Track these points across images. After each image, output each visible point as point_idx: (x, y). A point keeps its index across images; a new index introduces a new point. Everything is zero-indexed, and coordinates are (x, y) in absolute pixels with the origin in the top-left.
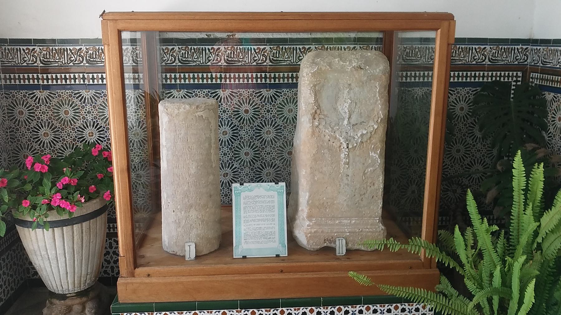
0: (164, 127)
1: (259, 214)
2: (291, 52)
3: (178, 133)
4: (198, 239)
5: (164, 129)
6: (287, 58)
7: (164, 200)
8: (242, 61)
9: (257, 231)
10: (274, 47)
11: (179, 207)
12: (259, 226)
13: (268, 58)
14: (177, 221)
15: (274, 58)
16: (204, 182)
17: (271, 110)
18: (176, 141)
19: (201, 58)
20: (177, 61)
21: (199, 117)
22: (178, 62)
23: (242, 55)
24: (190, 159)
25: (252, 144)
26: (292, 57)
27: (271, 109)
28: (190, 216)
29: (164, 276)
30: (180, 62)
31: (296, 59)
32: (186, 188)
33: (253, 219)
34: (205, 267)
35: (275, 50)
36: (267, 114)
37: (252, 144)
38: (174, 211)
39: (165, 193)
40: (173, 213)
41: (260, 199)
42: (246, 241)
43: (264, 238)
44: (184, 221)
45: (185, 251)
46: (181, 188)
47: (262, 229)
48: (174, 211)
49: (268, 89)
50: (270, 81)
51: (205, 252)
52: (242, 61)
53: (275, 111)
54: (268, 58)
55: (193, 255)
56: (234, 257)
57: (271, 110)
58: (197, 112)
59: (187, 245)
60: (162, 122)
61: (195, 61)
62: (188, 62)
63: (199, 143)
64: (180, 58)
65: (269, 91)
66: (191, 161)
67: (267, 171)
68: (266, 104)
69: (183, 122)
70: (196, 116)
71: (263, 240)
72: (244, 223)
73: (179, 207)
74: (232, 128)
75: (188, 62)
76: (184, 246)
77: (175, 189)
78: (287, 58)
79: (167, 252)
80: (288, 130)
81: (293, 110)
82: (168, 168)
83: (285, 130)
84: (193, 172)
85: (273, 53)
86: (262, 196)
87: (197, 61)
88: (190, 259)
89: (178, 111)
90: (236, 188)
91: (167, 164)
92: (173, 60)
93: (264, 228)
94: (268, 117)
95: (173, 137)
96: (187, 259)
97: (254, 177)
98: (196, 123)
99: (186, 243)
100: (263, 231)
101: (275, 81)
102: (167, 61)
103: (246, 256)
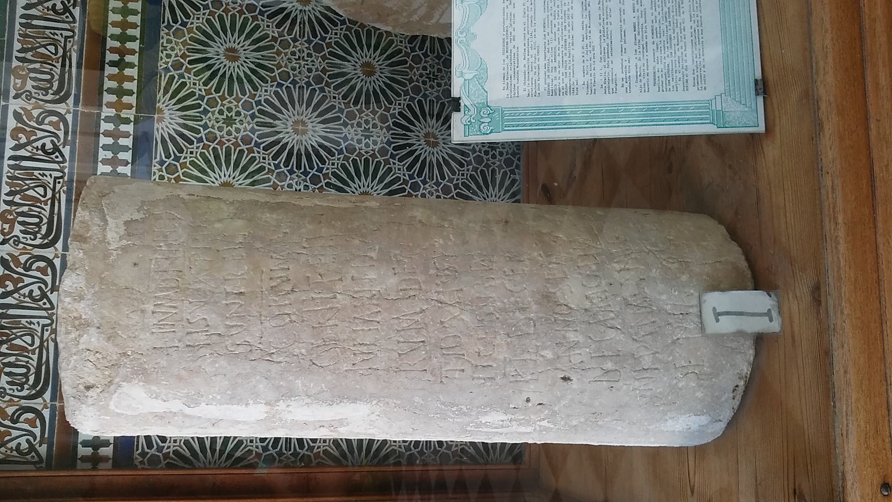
0: (176, 406)
1: (578, 32)
2: (38, 33)
3: (202, 338)
4: (684, 278)
5: (188, 411)
6: (56, 49)
7: (515, 427)
8: (54, 190)
9: (650, 40)
10: (15, 84)
11: (549, 354)
12: (630, 37)
13: (50, 107)
14: (609, 365)
15: (51, 88)
16: (441, 242)
17: (226, 112)
18: (241, 349)
19: (31, 323)
20: (37, 403)
21: (129, 235)
22: (40, 400)
23: (33, 188)
24: (330, 290)
25: (333, 180)
26: (54, 34)
27: (221, 112)
28: (588, 304)
29: (885, 412)
30: (39, 394)
31: (64, 22)
32: (466, 317)
33: (598, 56)
34: (840, 219)
35: (24, 84)
36: (238, 125)
37: (333, 180)
38: (565, 379)
39: (484, 419)
40: (575, 384)
41: (519, 33)
42: (691, 82)
43: (679, 12)
44: (612, 334)
45: (740, 334)
46: (464, 340)
47: (642, 20)
48: (565, 379)
49: (156, 116)
50: (130, 107)
51: (735, 255)
52: (54, 190)
53: (230, 102)
54: (50, 107)
55: (759, 300)
56: (761, 129)
57: (226, 112)
58: (104, 241)
59: (712, 326)
60: (160, 417)
61: (42, 342)
62: (44, 367)
63: (258, 245)
64: (25, 393)
65: (161, 111)
66: (339, 287)
67: (422, 142)
68: (205, 127)
69: (150, 307)
70: (124, 249)
71: (686, 16)
72: (614, 91)
73: (549, 354)
74: (236, 166)
75: (44, 367)
76: (718, 338)
77: (469, 371)
78: (56, 49)
79: (730, 424)
80: (294, 69)
81: (229, 45)
82: (372, 396)
83: (295, 76)
84: (393, 281)
85: (33, 91)
86: (507, 23)
87: (42, 338)
88: (774, 314)
89: (93, 330)
90: (468, 126)
91: (354, 400)
92: (30, 416)
93: (636, 14)
94: (249, 123)
95: (223, 362)
96: (775, 326)
97: (438, 184)
98: (155, 251)
99: (702, 329)
100: (650, 18)
101: (130, 93)
102: (35, 439)
103: (756, 81)
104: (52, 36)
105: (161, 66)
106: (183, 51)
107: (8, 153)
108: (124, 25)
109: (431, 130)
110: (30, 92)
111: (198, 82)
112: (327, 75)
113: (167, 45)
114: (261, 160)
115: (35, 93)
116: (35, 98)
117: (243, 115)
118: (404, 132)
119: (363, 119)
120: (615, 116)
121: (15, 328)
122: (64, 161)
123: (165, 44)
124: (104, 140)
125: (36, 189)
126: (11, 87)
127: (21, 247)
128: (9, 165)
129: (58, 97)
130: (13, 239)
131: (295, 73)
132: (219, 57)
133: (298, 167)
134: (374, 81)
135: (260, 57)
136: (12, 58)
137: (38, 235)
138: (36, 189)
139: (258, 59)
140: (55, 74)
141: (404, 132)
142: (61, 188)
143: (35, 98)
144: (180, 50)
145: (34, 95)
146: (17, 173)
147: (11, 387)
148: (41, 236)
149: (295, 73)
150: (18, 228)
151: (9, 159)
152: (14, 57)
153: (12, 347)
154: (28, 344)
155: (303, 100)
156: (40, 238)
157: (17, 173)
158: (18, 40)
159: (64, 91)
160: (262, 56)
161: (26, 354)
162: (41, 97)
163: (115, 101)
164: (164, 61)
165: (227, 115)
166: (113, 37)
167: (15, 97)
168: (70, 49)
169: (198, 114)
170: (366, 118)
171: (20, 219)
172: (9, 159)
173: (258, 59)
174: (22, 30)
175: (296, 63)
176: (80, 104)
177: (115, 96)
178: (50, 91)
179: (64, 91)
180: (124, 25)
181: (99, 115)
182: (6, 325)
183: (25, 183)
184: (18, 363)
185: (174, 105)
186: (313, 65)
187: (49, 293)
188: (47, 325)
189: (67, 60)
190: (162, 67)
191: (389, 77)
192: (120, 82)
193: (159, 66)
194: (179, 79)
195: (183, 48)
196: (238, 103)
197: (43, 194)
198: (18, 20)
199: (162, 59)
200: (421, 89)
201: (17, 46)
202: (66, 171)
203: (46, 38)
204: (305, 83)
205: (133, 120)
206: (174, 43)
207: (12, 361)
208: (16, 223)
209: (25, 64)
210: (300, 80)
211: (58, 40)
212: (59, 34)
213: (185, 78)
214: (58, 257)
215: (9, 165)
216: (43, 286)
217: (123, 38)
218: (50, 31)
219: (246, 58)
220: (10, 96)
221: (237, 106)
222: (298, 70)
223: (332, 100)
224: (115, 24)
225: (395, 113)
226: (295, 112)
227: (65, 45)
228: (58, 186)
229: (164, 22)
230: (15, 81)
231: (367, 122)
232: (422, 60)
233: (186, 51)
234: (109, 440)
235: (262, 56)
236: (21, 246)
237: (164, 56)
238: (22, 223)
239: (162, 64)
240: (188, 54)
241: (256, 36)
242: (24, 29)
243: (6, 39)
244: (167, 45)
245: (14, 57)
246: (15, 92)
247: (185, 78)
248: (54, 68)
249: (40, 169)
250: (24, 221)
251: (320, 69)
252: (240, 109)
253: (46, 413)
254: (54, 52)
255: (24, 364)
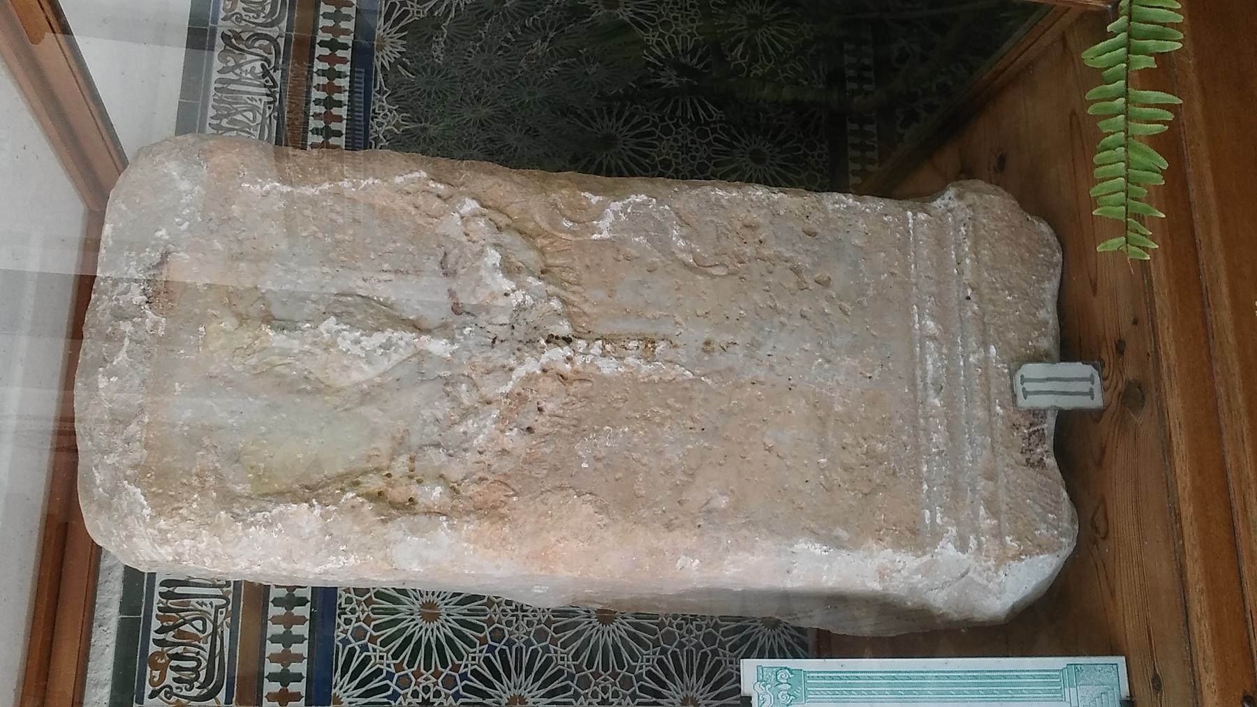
6: (204, 625)
15: (197, 679)
17: (421, 694)
22: (276, 28)
23: (241, 113)
26: (202, 604)
57: (421, 694)
62: (217, 659)
75: (217, 659)
78: (204, 625)
83: (511, 633)
87: (215, 622)
104: (200, 608)
105: (338, 636)
106: (366, 613)
107: (215, 76)
108: (286, 658)
109: (690, 694)
110: (241, 15)
111: (385, 654)
112: (552, 628)
113: (346, 606)
114: (471, 655)
115: (177, 688)
116: (245, 20)
117: (443, 695)
118: (655, 699)
119: (600, 686)
120: (943, 685)
121: (237, 103)
122: (275, 86)
123: (377, 111)
124: (319, 65)
125: (244, 114)
126: (147, 682)
127: (174, 701)
128: (161, 594)
129: (206, 691)
130: (163, 691)
131: (511, 629)
132: (413, 617)
133: (519, 650)
134: (613, 631)
135: (466, 611)
136: (205, 125)
137: (195, 683)
138: (244, 114)
139: (464, 615)
140: (202, 659)
141: (655, 699)
142: (224, 619)
143: (245, 20)
144: (363, 611)
145: (175, 691)
146: (171, 603)
147: (177, 685)
148: (199, 685)
149: (511, 629)
150: (171, 674)
151: (162, 584)
152: (151, 641)
153: (182, 635)
154: (249, 120)
155: (521, 667)
156: (198, 688)
157: (171, 603)
158: (213, 107)
159: (214, 682)
160: (468, 610)
161: (197, 643)
162: (184, 693)
163: (280, 671)
164: (341, 629)
165: (423, 698)
166: (318, 87)
167: (151, 697)
168: (222, 623)
169: (386, 700)
170: (603, 684)
171: (174, 663)
172: (162, 584)
173: (464, 615)
174: (162, 603)
175: (512, 616)
176: (234, 699)
177: (282, 626)
178: (196, 684)
179: (214, 682)
180: (329, 117)
181: (314, 39)
182: (172, 606)
183: (180, 616)
184: (187, 654)
185: (355, 689)
186: (534, 616)
187: (271, 72)
188: (222, 607)
189: (218, 639)
190: (339, 638)
191: (633, 623)
192: (287, 645)
193: (335, 637)
194: (361, 653)
195: (366, 609)
196: (437, 679)
197: (201, 629)
198: (213, 86)
199: (339, 626)
200: (675, 636)
201: (156, 624)
202: (230, 597)
203: (192, 610)
204: (524, 643)
205: (351, 45)
206: (355, 602)
207: (179, 652)
208: (169, 669)
209: (166, 649)
210: (517, 638)
211: (205, 612)
212: (208, 603)
213: (407, 6)
214: (282, 37)
215: (161, 594)
216: (266, 65)
217: (329, 103)
218: (197, 600)
219: (448, 615)
220: (146, 695)
221: (436, 684)
222: (515, 625)
223: (560, 662)
224: (325, 29)
225: (642, 673)
226: (511, 685)
227: (216, 617)
228: (221, 618)
229: (375, 87)
230: (151, 672)
231: (605, 690)
232: (672, 131)
233: (370, 613)
234: (299, 693)
235: (468, 610)
236: (244, 23)
237: (341, 622)
238: (177, 669)
239: (340, 634)
240: (373, 616)
241: (459, 643)
242: (164, 601)
243: (142, 616)
244: (346, 606)
245: (151, 641)
246: (152, 688)
247: (407, 6)
248: (201, 651)
249: (248, 93)
250: (178, 666)
251: (544, 620)
252: (440, 687)
253: (282, 42)
254: (201, 629)
255: (194, 655)
